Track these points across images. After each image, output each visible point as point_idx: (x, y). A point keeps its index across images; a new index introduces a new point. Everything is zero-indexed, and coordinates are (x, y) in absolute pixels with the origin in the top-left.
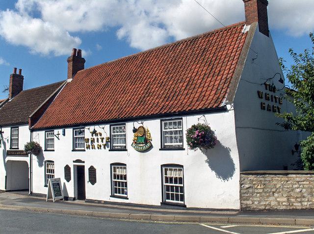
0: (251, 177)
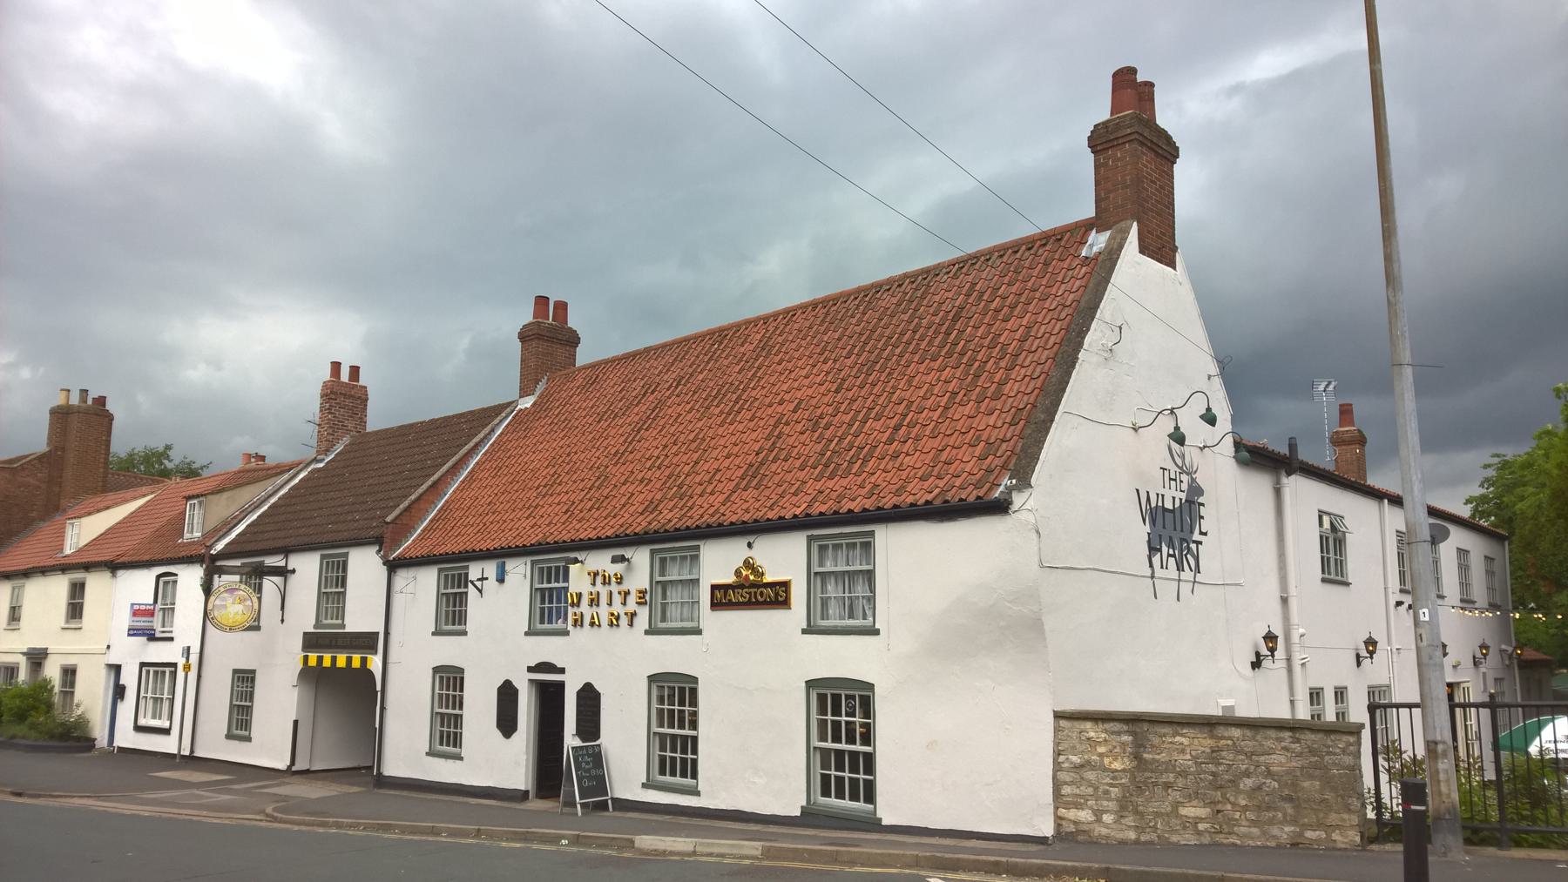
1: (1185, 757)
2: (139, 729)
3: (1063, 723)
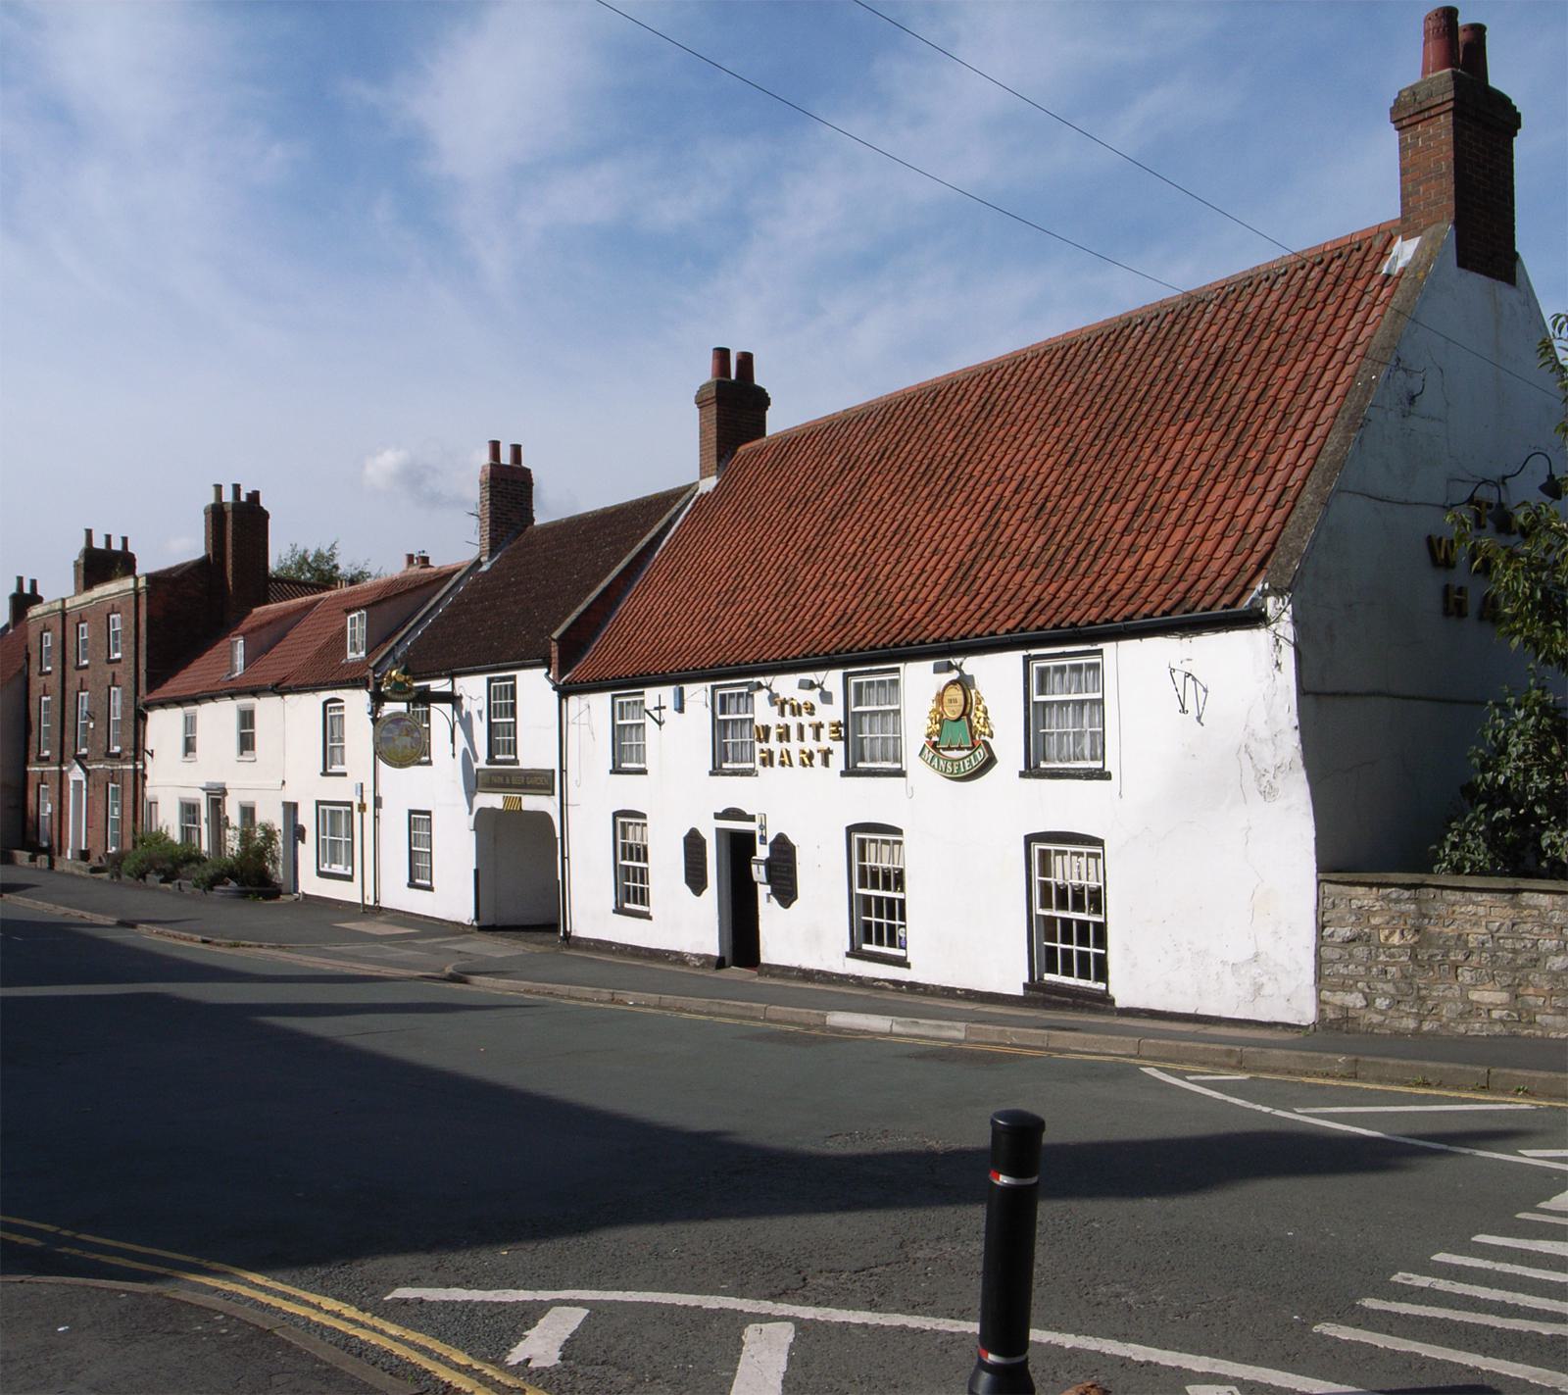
0: (1364, 897)
1: (1479, 931)
2: (321, 874)
3: (1328, 888)
